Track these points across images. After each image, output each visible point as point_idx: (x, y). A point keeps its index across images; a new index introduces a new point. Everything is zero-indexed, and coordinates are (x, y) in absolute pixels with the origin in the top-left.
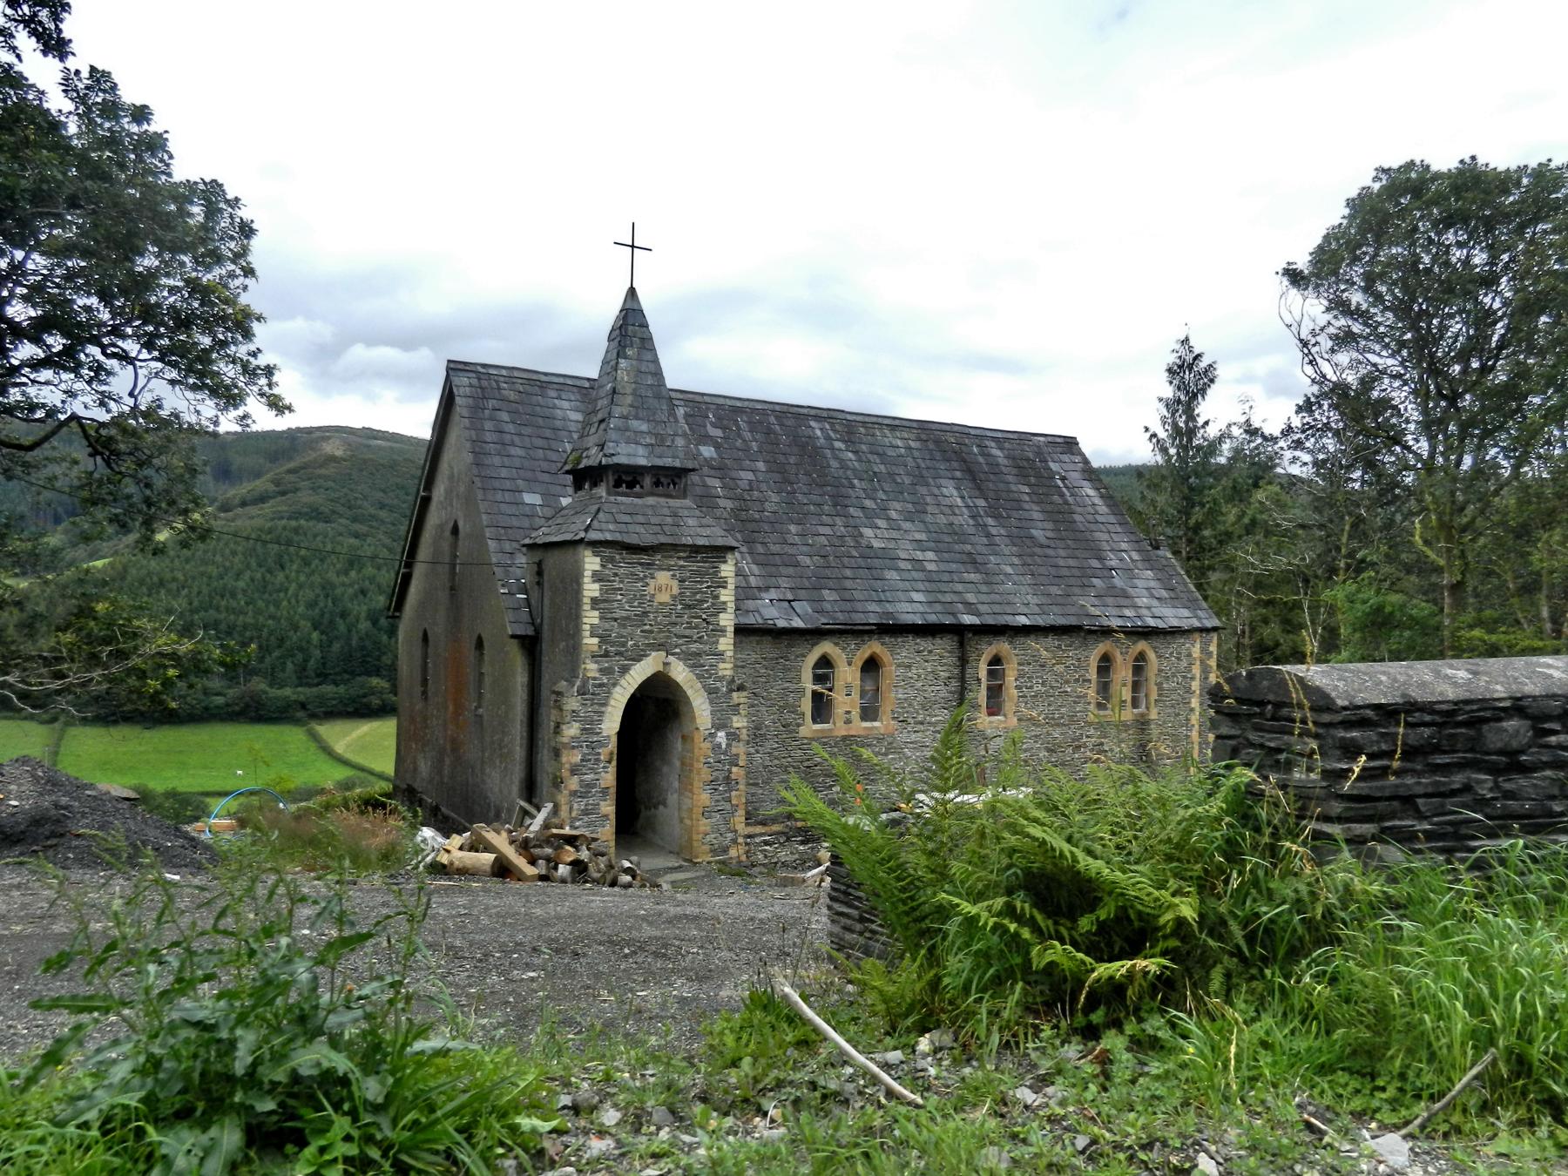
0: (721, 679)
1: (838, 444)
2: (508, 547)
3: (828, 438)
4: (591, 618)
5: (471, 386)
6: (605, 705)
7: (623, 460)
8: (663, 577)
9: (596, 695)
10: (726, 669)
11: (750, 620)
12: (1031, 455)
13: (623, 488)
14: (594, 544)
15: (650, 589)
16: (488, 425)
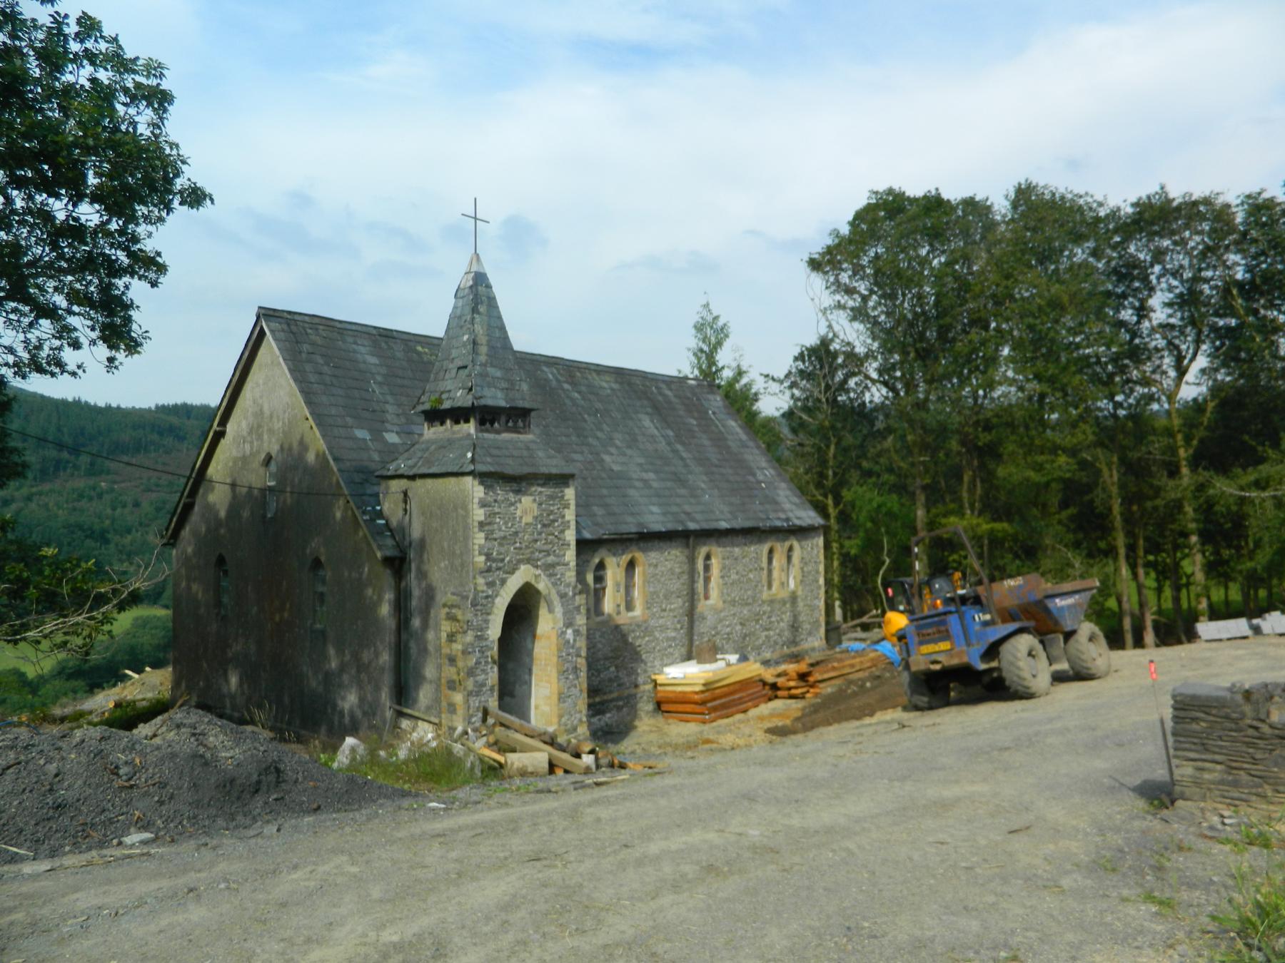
0: (568, 585)
1: (566, 386)
3: (558, 380)
5: (283, 331)
6: (489, 614)
7: (490, 402)
9: (481, 605)
10: (571, 576)
12: (689, 395)
13: (488, 425)
15: (519, 513)
16: (308, 367)
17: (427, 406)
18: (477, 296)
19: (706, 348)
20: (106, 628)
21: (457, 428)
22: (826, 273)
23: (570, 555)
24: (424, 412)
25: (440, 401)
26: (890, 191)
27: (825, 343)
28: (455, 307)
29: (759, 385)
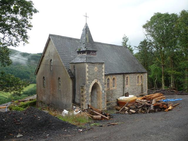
2: (66, 63)
4: (87, 74)
8: (96, 68)
9: (88, 87)
10: (104, 81)
11: (106, 74)
13: (88, 54)
14: (87, 63)
15: (94, 70)
17: (78, 51)
18: (87, 31)
19: (124, 42)
20: (23, 90)
21: (83, 54)
22: (146, 28)
23: (103, 77)
24: (77, 52)
25: (80, 49)
26: (158, 13)
27: (145, 41)
28: (83, 33)
29: (133, 48)
